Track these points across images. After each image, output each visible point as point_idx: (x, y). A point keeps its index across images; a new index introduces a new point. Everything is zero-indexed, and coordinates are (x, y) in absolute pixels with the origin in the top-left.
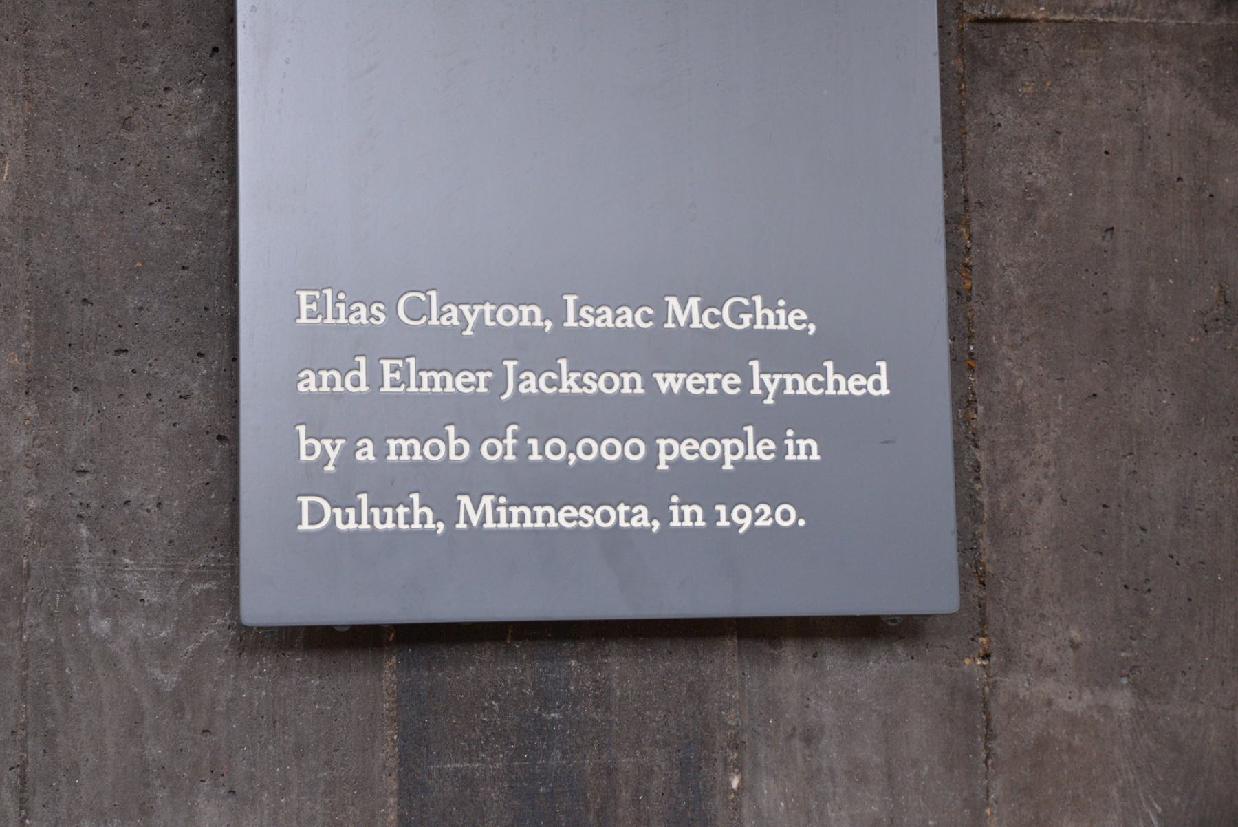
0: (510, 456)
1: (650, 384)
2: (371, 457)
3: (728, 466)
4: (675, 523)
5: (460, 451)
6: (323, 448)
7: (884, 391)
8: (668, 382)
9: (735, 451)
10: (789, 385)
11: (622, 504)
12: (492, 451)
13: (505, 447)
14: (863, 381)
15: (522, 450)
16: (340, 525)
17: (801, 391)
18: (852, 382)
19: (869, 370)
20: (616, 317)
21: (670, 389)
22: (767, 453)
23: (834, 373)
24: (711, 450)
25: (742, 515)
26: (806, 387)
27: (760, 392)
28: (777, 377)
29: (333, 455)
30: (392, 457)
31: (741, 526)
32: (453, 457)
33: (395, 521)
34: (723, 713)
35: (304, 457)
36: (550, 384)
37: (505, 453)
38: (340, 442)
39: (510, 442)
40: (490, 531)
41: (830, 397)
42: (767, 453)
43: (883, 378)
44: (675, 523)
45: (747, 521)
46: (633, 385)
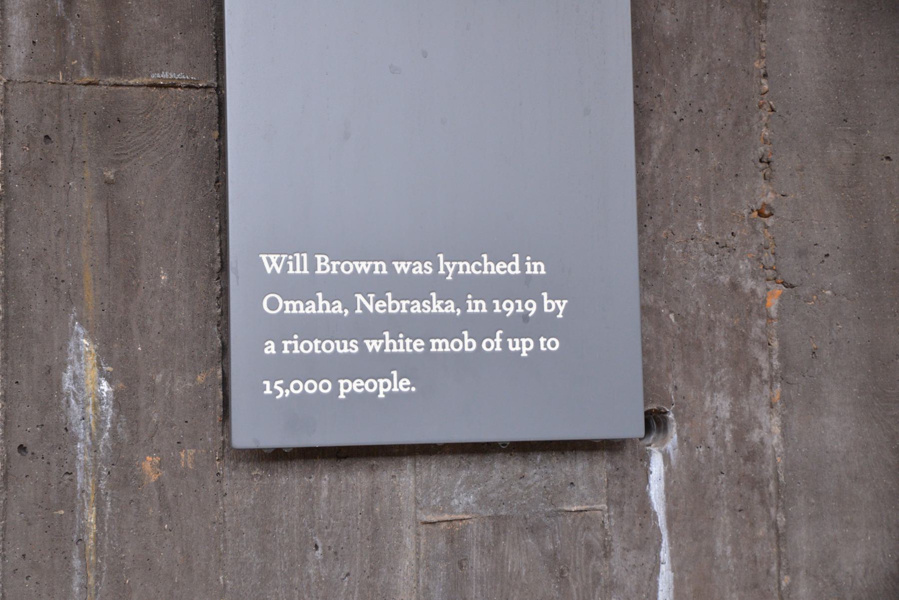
0: (498, 349)
1: (391, 268)
2: (273, 352)
4: (470, 310)
5: (470, 345)
6: (556, 305)
8: (401, 267)
9: (385, 386)
10: (377, 268)
11: (317, 340)
12: (488, 345)
13: (495, 343)
14: (505, 266)
15: (504, 345)
16: (339, 350)
17: (468, 272)
18: (498, 267)
22: (419, 347)
23: (488, 261)
24: (371, 386)
25: (508, 306)
27: (444, 273)
28: (454, 264)
29: (562, 309)
30: (433, 349)
32: (467, 349)
33: (405, 347)
35: (546, 310)
36: (477, 268)
37: (495, 347)
38: (565, 302)
39: (498, 340)
40: (388, 354)
41: (486, 275)
42: (419, 347)
44: (470, 310)
45: (511, 309)
46: (539, 269)
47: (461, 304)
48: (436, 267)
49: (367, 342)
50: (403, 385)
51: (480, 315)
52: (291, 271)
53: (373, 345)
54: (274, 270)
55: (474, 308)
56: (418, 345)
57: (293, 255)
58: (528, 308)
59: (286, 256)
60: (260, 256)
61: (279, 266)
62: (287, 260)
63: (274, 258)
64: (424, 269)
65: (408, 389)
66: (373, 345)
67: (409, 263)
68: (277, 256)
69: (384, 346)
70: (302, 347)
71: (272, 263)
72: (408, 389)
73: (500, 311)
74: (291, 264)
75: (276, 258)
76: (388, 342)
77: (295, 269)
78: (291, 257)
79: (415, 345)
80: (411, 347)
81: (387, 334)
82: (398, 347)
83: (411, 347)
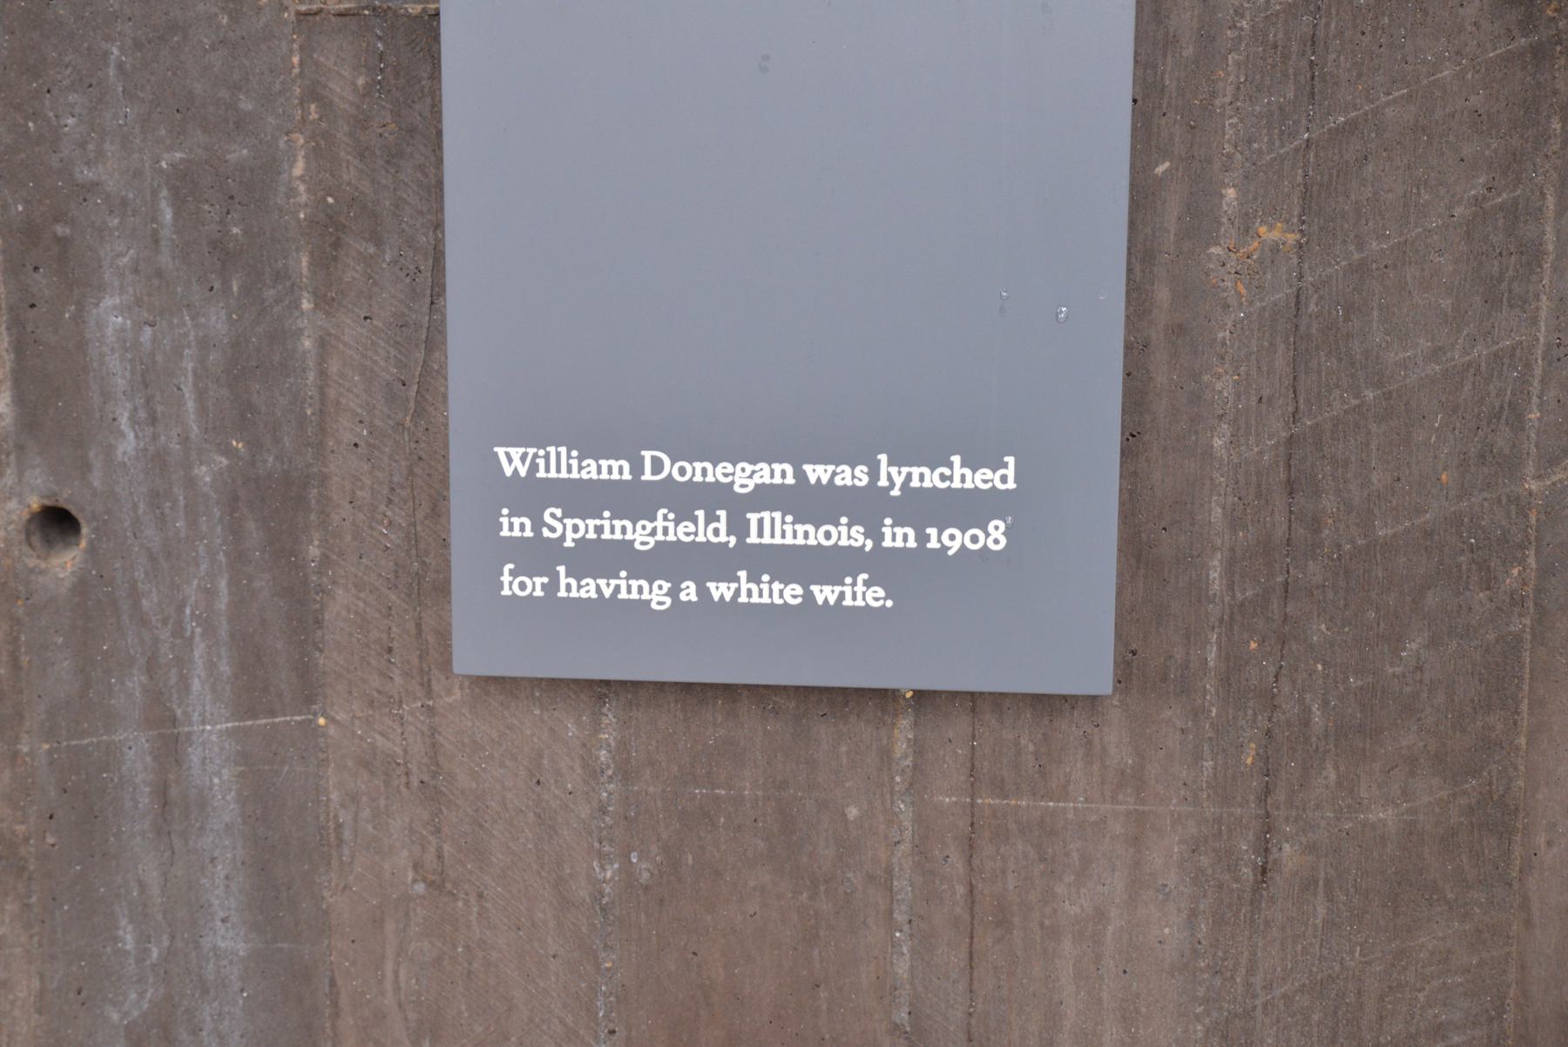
1: (800, 475)
2: (694, 598)
3: (569, 544)
4: (887, 543)
7: (1011, 485)
8: (817, 473)
14: (989, 474)
17: (927, 484)
18: (719, 470)
19: (998, 465)
20: (579, 587)
21: (819, 479)
22: (794, 597)
25: (952, 537)
26: (931, 478)
28: (905, 470)
31: (950, 548)
33: (771, 596)
34: (55, 756)
36: (943, 478)
42: (794, 597)
43: (1010, 472)
44: (887, 543)
47: (874, 533)
48: (874, 474)
49: (711, 585)
50: (875, 597)
51: (905, 550)
52: (541, 474)
53: (720, 590)
54: (516, 471)
55: (894, 539)
56: (792, 594)
57: (545, 449)
58: (946, 542)
59: (535, 450)
60: (496, 449)
61: (523, 463)
62: (536, 456)
63: (516, 452)
64: (853, 477)
65: (881, 602)
66: (720, 590)
67: (831, 468)
68: (522, 450)
69: (737, 592)
70: (515, 587)
71: (512, 460)
72: (881, 602)
73: (938, 546)
74: (541, 462)
75: (520, 454)
76: (744, 586)
77: (547, 470)
78: (542, 452)
79: (869, 595)
80: (781, 596)
81: (743, 574)
82: (761, 595)
83: (781, 596)
